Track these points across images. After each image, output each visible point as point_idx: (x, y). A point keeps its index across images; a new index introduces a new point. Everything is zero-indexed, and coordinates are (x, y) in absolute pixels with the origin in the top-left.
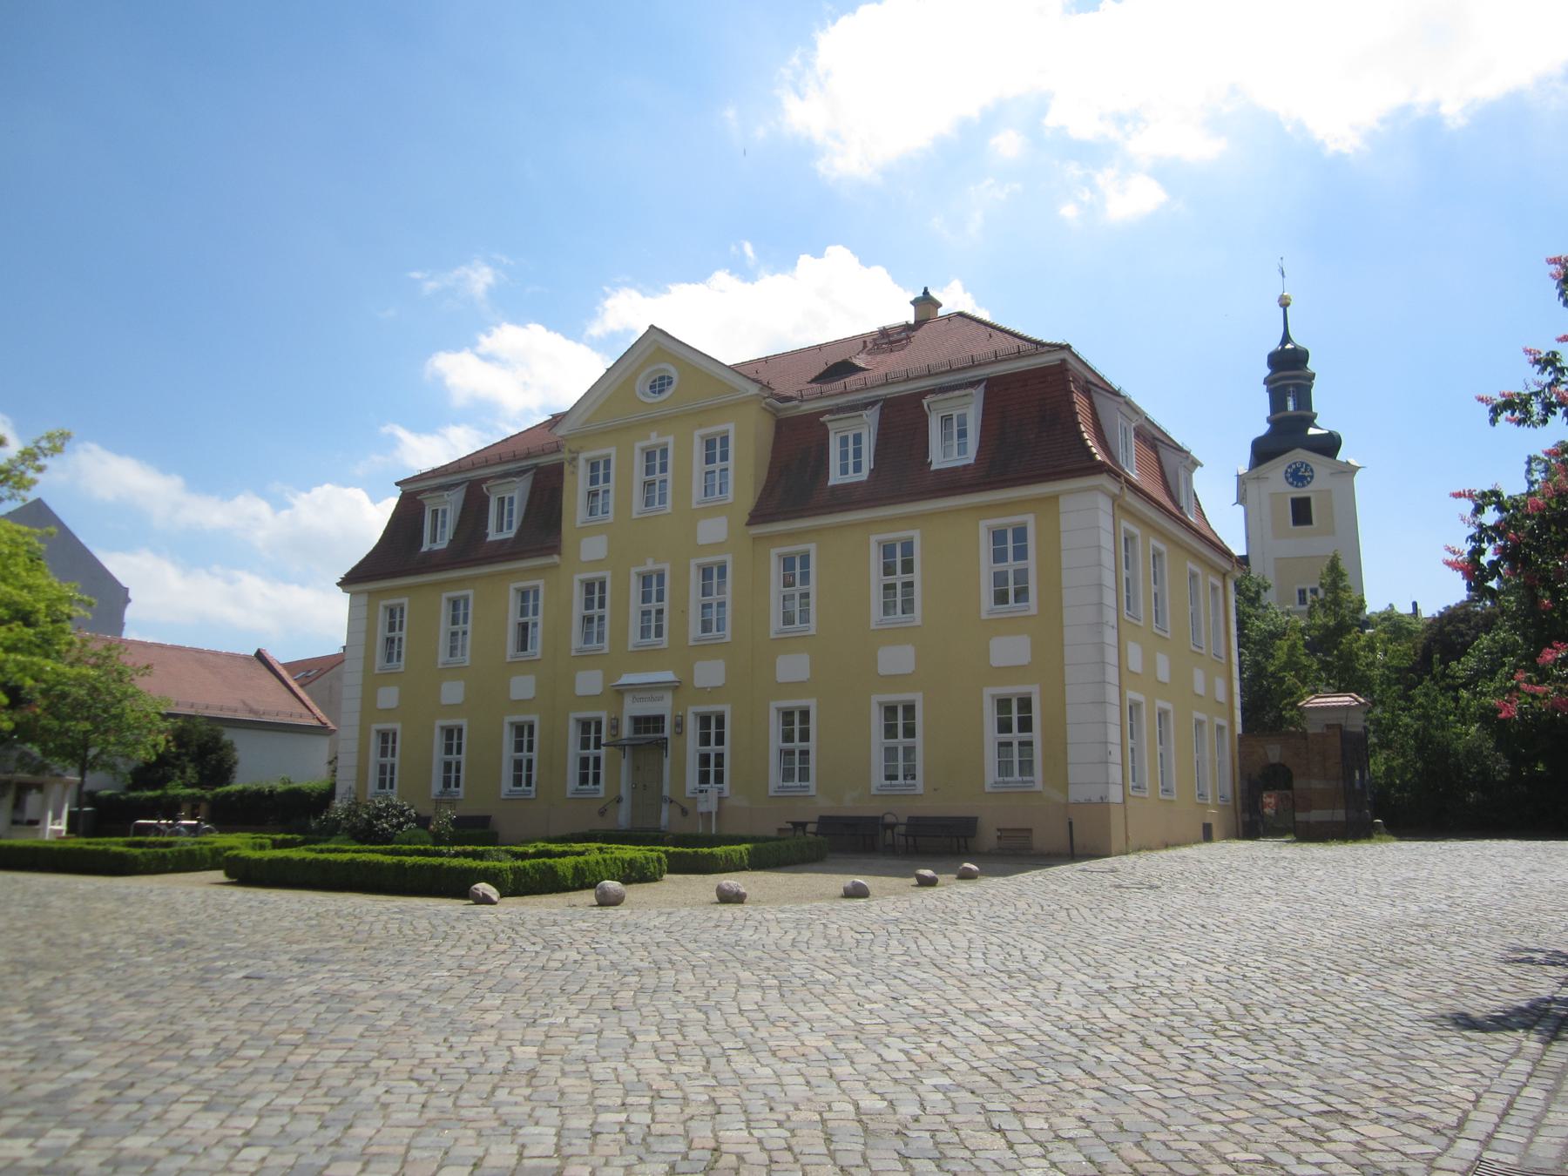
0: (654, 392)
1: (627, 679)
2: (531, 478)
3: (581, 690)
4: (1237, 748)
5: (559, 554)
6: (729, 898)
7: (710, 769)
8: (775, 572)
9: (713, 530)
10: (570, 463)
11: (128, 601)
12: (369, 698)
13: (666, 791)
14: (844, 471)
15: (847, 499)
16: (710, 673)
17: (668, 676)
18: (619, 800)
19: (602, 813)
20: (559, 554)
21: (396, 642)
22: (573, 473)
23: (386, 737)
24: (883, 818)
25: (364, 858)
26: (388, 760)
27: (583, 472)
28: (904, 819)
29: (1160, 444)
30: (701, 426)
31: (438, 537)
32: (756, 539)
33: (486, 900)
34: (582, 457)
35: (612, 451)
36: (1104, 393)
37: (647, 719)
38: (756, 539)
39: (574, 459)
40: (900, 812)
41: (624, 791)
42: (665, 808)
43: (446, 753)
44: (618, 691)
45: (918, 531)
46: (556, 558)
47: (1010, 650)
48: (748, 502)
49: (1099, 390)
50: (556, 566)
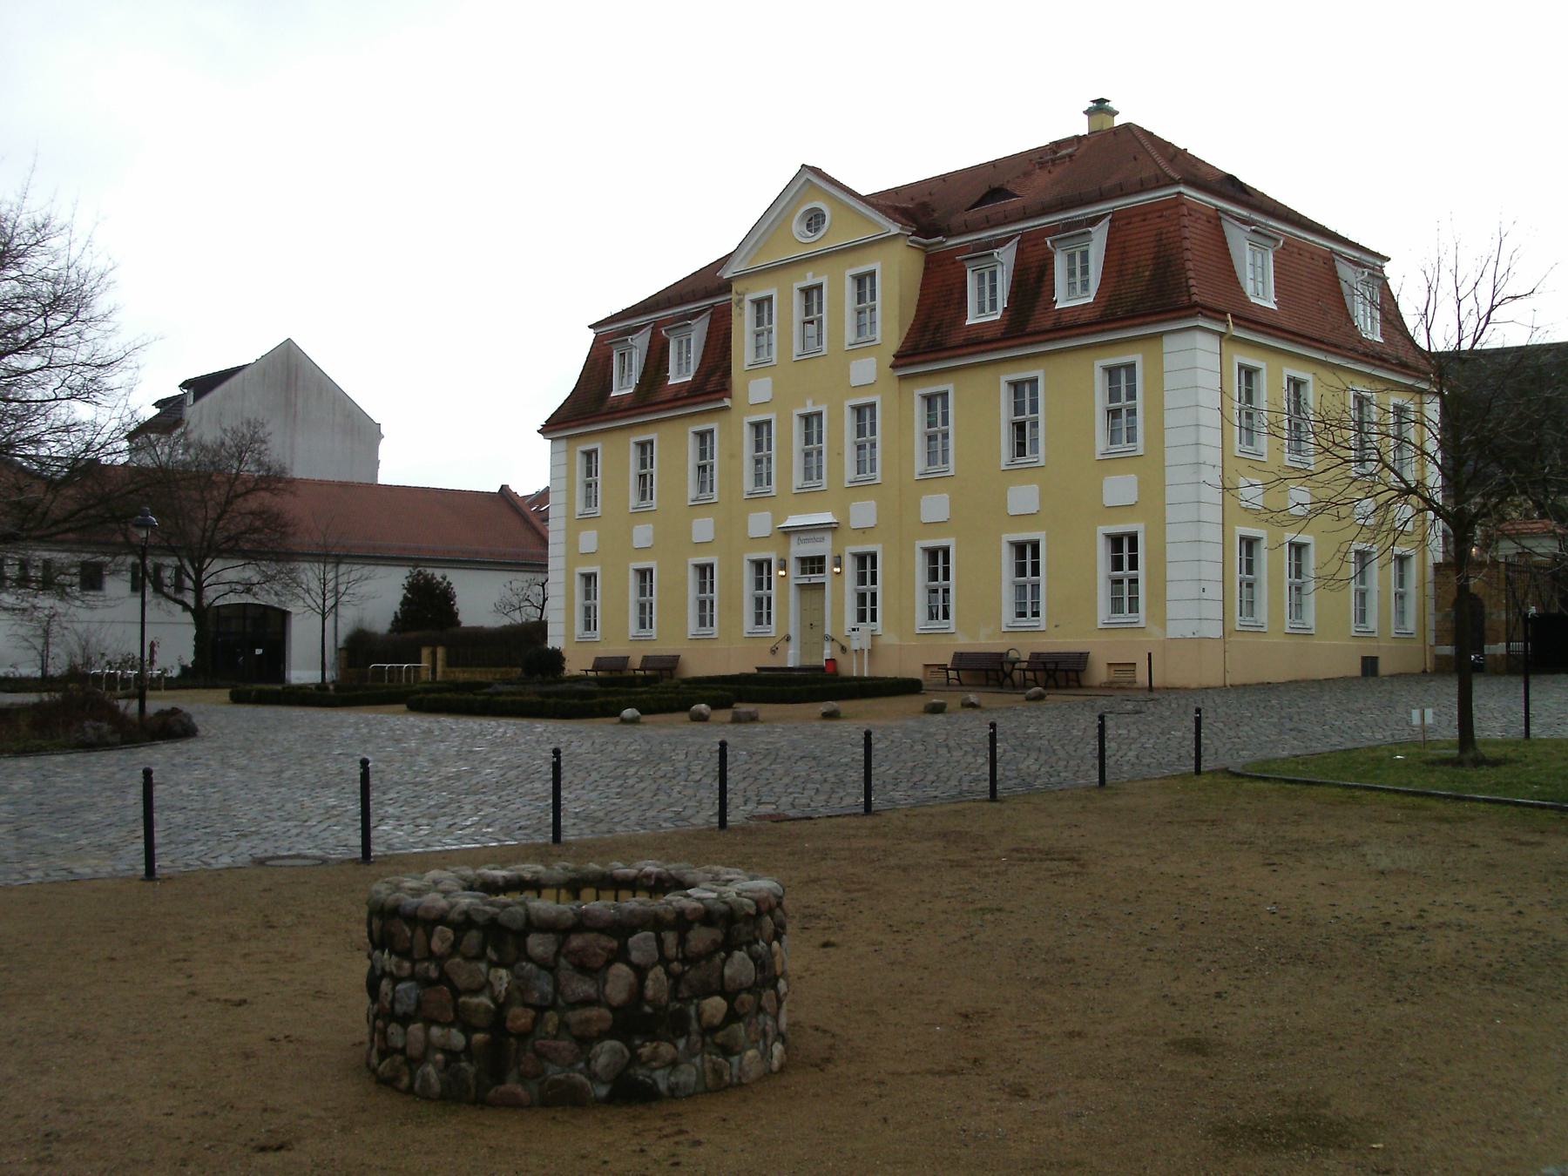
0: (810, 231)
1: (794, 521)
2: (707, 321)
3: (754, 531)
4: (1430, 589)
5: (730, 397)
6: (831, 716)
7: (866, 608)
8: (919, 409)
9: (866, 370)
10: (737, 305)
11: (380, 436)
12: (572, 543)
13: (828, 631)
14: (982, 310)
15: (980, 341)
16: (863, 513)
17: (826, 518)
18: (788, 639)
19: (774, 651)
20: (730, 397)
21: (593, 486)
22: (740, 315)
23: (589, 578)
24: (1008, 653)
25: (764, 810)
26: (591, 602)
27: (749, 311)
28: (1025, 657)
29: (1337, 258)
30: (851, 266)
31: (623, 387)
32: (902, 378)
33: (634, 721)
34: (749, 297)
35: (823, 279)
36: (1231, 220)
37: (812, 560)
38: (902, 378)
39: (741, 301)
40: (1024, 648)
41: (793, 631)
42: (827, 645)
43: (641, 596)
44: (785, 533)
45: (1042, 371)
46: (727, 402)
47: (1120, 489)
48: (894, 345)
49: (1227, 218)
50: (727, 408)
